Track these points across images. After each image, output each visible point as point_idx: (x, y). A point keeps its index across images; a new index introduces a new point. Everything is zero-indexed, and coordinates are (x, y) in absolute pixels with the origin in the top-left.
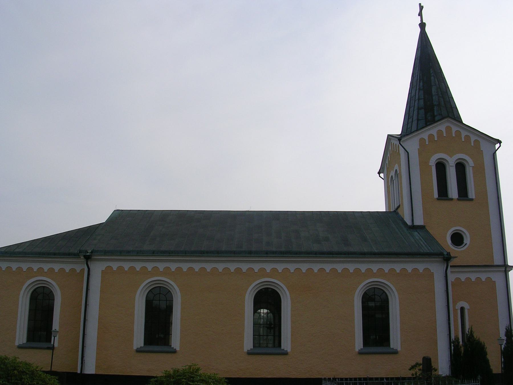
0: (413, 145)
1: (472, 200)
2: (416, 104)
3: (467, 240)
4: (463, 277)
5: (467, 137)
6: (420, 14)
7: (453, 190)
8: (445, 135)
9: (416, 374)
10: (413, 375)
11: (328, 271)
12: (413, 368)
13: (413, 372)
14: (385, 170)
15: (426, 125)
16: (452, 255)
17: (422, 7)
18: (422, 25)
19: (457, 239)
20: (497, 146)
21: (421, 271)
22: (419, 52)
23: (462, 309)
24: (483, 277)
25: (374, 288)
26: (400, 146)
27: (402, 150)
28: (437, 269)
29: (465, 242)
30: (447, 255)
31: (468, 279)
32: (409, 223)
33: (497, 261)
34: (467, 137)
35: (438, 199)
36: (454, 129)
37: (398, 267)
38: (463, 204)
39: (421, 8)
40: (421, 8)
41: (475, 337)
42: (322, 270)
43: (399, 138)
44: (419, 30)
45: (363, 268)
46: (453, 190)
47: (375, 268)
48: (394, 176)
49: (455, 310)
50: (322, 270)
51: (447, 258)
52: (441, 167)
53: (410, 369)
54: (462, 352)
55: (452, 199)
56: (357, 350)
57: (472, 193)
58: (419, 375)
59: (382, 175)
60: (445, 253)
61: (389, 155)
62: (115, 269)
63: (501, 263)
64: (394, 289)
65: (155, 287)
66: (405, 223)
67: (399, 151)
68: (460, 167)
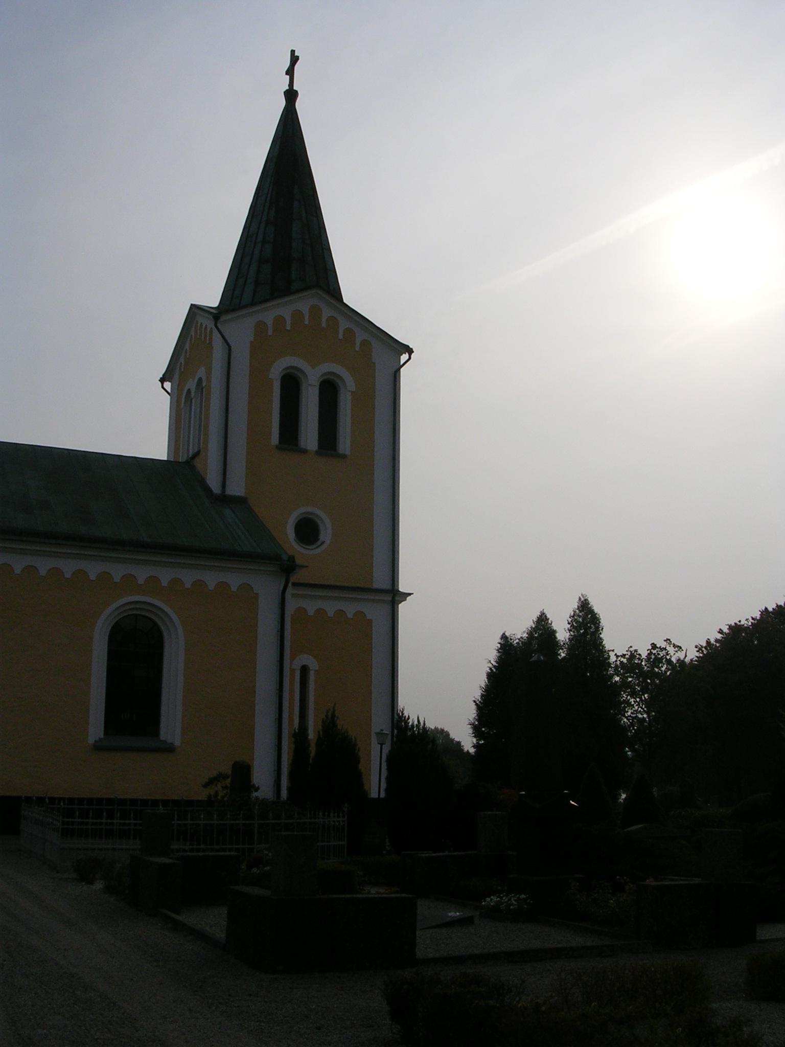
0: (241, 331)
1: (343, 457)
2: (257, 252)
3: (326, 535)
4: (311, 607)
5: (349, 333)
6: (290, 72)
7: (309, 435)
8: (307, 322)
9: (216, 794)
10: (210, 797)
11: (43, 573)
12: (211, 782)
13: (211, 791)
14: (176, 376)
15: (272, 297)
16: (298, 561)
17: (297, 58)
18: (291, 95)
19: (308, 531)
20: (404, 357)
21: (234, 589)
22: (278, 147)
23: (304, 670)
24: (350, 609)
25: (136, 615)
26: (215, 330)
27: (217, 337)
28: (265, 587)
29: (322, 537)
30: (289, 560)
31: (321, 612)
32: (216, 488)
33: (380, 581)
34: (349, 333)
35: (277, 447)
36: (327, 312)
37: (188, 577)
39: (294, 59)
40: (294, 59)
41: (339, 727)
42: (31, 569)
43: (217, 314)
44: (282, 103)
45: (118, 572)
46: (309, 435)
47: (142, 574)
48: (193, 391)
49: (293, 671)
50: (31, 569)
51: (287, 568)
52: (291, 384)
53: (205, 786)
54: (313, 754)
55: (305, 451)
56: (91, 740)
57: (345, 444)
58: (223, 797)
59: (168, 385)
60: (285, 557)
61: (187, 347)
62: (117, 579)
63: (386, 585)
65: (147, 617)
66: (208, 490)
67: (211, 339)
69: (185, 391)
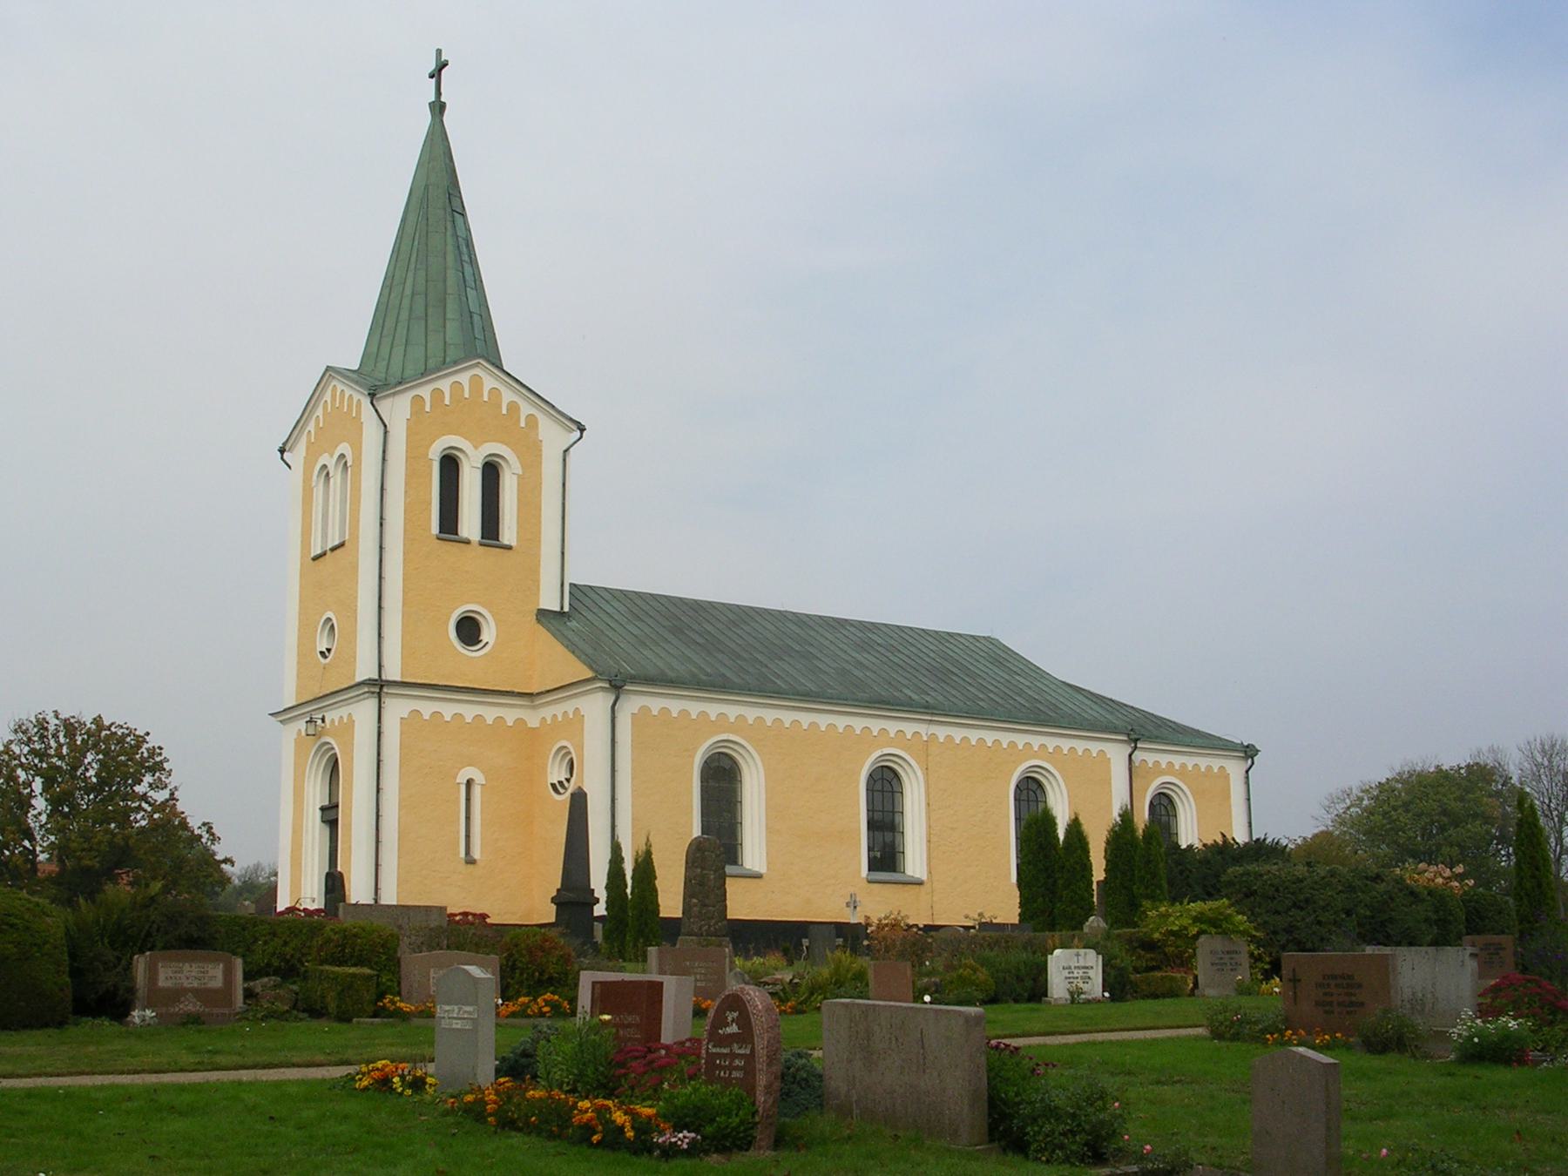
3: (488, 634)
18: (438, 108)
23: (469, 783)
36: (489, 382)
38: (480, 559)
40: (442, 65)
52: (450, 465)
55: (467, 542)
64: (1184, 787)
68: (491, 472)
69: (318, 467)
